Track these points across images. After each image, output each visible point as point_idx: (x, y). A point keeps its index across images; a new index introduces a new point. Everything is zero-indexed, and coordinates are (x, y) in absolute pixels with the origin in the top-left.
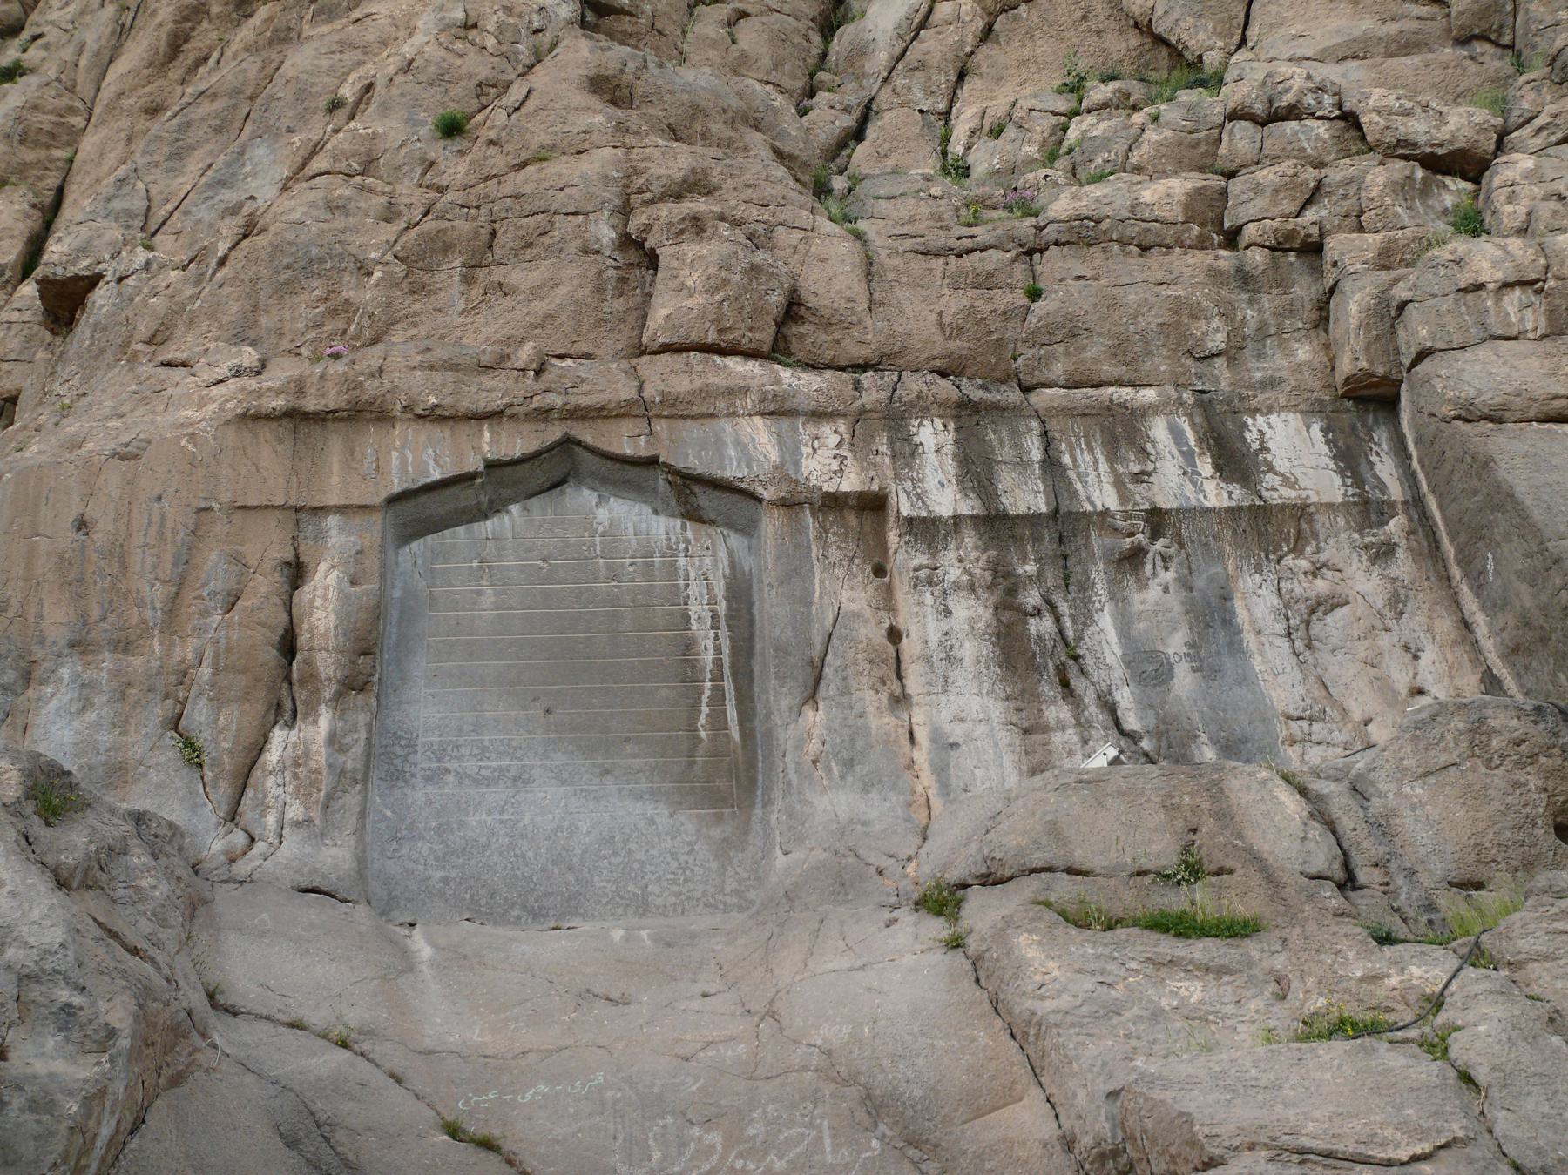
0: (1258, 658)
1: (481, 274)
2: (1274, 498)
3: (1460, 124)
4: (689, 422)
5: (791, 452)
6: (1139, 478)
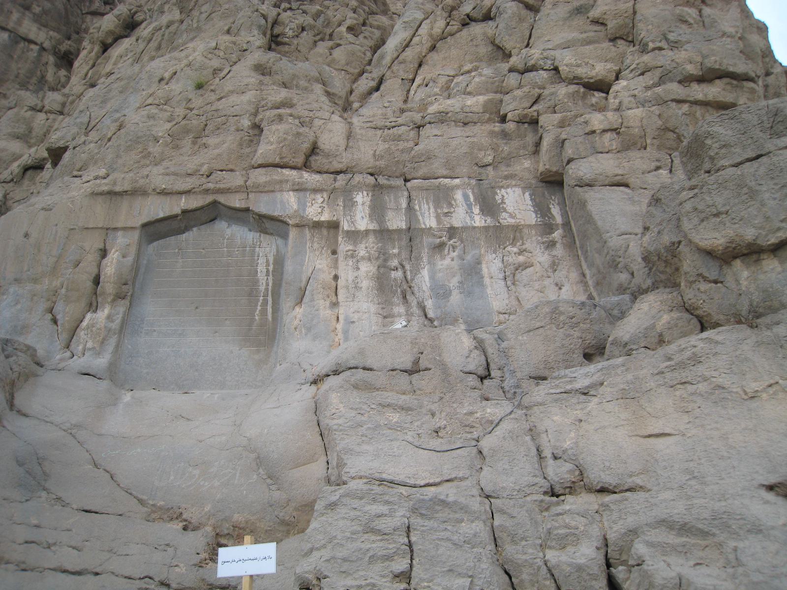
0: (490, 288)
1: (199, 140)
2: (504, 222)
3: (600, 70)
4: (263, 194)
5: (302, 205)
6: (446, 214)
